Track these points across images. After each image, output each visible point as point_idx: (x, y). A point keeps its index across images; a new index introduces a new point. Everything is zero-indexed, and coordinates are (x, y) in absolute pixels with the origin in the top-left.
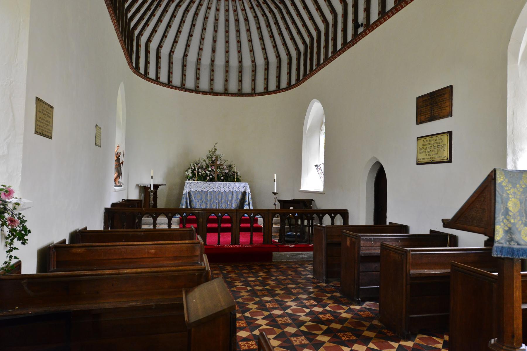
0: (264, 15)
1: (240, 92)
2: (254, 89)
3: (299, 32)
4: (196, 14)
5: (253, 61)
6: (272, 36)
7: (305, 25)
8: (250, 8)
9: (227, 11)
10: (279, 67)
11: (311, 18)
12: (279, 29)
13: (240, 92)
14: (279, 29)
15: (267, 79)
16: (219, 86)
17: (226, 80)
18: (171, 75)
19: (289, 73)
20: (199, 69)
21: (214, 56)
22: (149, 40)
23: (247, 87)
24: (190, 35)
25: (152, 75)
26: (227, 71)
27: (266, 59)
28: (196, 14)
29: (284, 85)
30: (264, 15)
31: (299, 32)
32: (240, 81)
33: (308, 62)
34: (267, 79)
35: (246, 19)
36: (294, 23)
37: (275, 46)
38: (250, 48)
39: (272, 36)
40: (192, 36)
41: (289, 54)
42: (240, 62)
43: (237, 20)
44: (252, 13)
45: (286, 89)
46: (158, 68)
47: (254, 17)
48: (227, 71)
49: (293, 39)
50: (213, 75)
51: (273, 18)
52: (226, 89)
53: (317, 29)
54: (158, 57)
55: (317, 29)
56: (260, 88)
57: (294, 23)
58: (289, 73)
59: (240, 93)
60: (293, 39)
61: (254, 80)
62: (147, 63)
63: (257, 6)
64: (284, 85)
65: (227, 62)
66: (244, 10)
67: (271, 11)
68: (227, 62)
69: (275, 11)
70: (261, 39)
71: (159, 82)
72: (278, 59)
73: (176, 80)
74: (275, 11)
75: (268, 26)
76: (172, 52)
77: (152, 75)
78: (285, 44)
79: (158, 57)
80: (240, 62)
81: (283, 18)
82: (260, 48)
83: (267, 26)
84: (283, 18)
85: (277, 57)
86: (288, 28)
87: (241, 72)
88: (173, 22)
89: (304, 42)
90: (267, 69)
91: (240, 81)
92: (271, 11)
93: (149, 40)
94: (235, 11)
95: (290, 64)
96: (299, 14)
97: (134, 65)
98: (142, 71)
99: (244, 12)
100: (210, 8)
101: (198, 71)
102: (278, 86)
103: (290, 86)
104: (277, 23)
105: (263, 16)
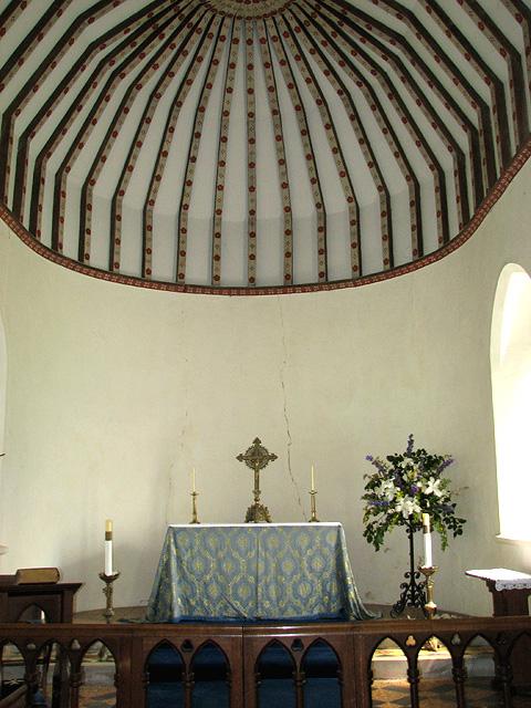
0: (362, 82)
1: (323, 280)
2: (358, 268)
3: (451, 103)
4: (177, 103)
5: (352, 199)
6: (388, 129)
7: (459, 78)
8: (326, 73)
9: (272, 89)
10: (416, 204)
11: (472, 53)
12: (402, 107)
13: (323, 280)
14: (402, 107)
15: (388, 237)
16: (270, 271)
17: (288, 255)
18: (147, 256)
19: (443, 213)
20: (218, 235)
21: (218, 247)
22: (65, 167)
23: (340, 265)
24: (137, 142)
25: (70, 249)
26: (288, 233)
27: (383, 187)
28: (177, 103)
29: (432, 244)
30: (362, 82)
31: (451, 103)
32: (323, 252)
33: (484, 169)
34: (388, 237)
35: (322, 101)
36: (434, 82)
37: (400, 153)
38: (203, 117)
39: (388, 129)
40: (166, 154)
41: (435, 165)
42: (320, 205)
43: (300, 108)
44: (332, 83)
45: (438, 255)
46: (84, 231)
47: (340, 93)
48: (288, 233)
49: (438, 123)
50: (253, 246)
51: (383, 85)
52: (288, 277)
53: (491, 77)
54: (85, 206)
55: (491, 77)
56: (374, 263)
57: (434, 82)
58: (443, 213)
59: (324, 282)
60: (438, 123)
61: (357, 245)
62: (57, 219)
63: (341, 64)
64: (432, 244)
65: (288, 209)
66: (311, 79)
67: (376, 69)
68: (288, 209)
69: (386, 66)
70: (364, 140)
71: (62, 256)
72: (412, 182)
73: (98, 256)
74: (386, 66)
75: (376, 105)
76: (90, 180)
77: (70, 249)
78: (422, 142)
79: (85, 206)
80: (320, 205)
81: (407, 78)
82: (372, 165)
83: (373, 108)
84: (407, 78)
85: (408, 178)
86: (422, 100)
87: (322, 229)
88: (121, 123)
89: (467, 124)
90: (387, 214)
91: (323, 252)
92: (376, 69)
93: (65, 167)
94: (292, 86)
95: (441, 189)
96: (441, 56)
97: (26, 224)
98: (46, 239)
99: (313, 85)
100: (210, 86)
101: (323, 270)
102: (419, 250)
103: (448, 244)
104: (393, 94)
105: (359, 84)
